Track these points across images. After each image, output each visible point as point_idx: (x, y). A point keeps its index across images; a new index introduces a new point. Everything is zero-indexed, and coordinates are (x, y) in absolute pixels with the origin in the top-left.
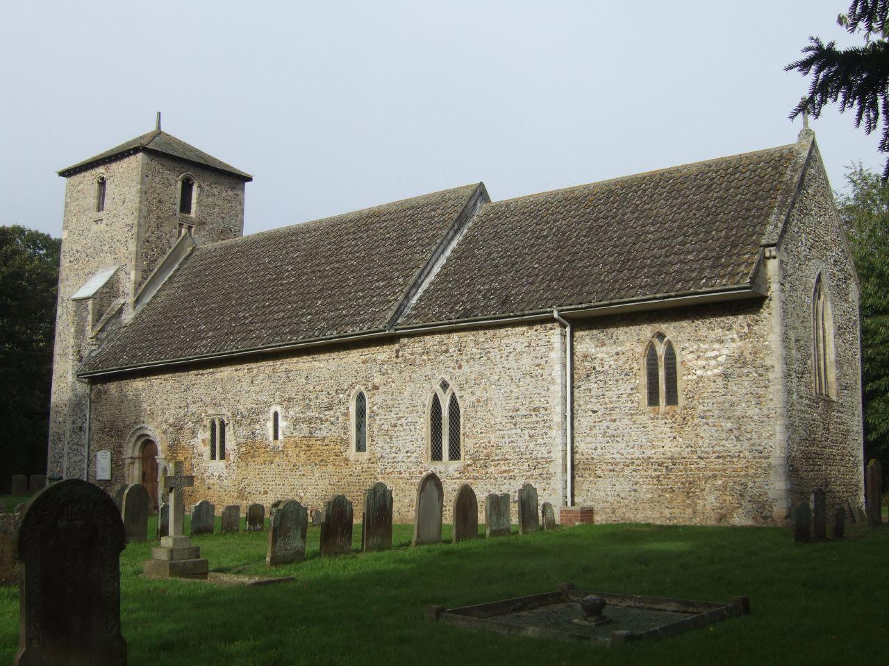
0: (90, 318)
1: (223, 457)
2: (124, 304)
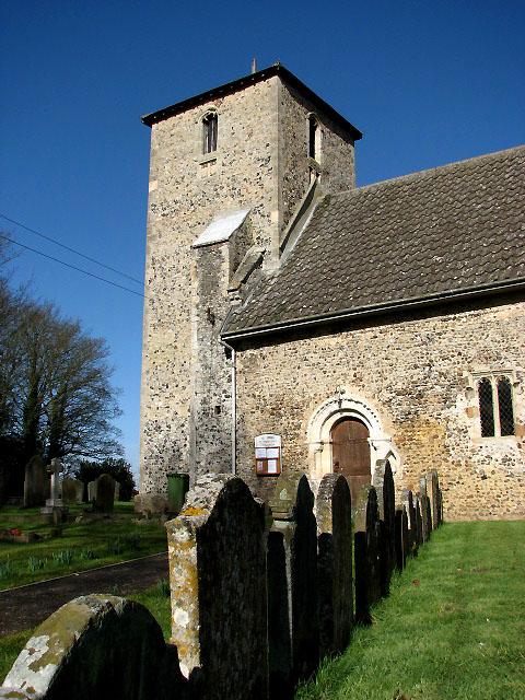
0: (226, 266)
1: (508, 429)
2: (263, 253)
